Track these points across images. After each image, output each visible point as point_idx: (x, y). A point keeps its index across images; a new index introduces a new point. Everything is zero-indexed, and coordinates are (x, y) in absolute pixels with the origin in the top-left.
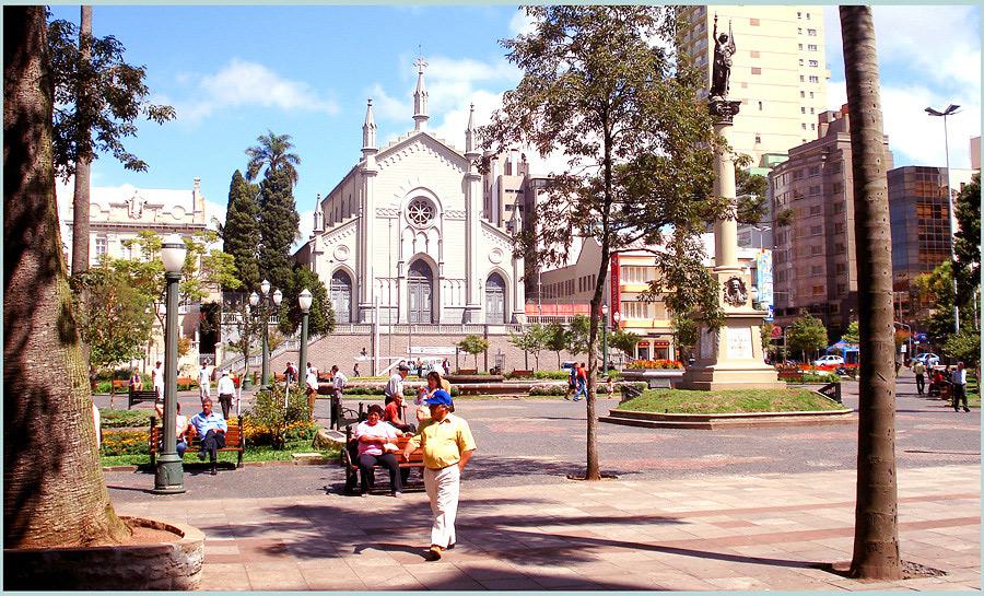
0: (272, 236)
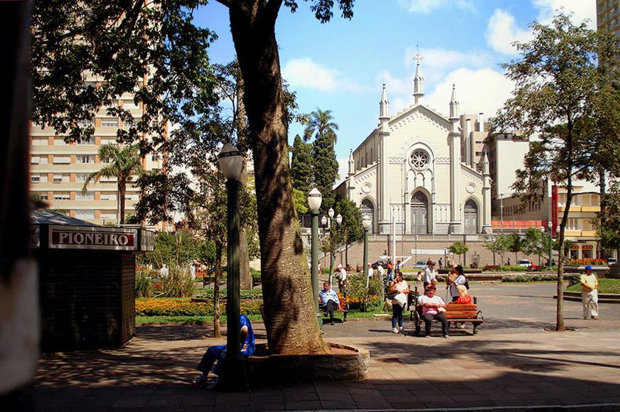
0: (321, 177)
